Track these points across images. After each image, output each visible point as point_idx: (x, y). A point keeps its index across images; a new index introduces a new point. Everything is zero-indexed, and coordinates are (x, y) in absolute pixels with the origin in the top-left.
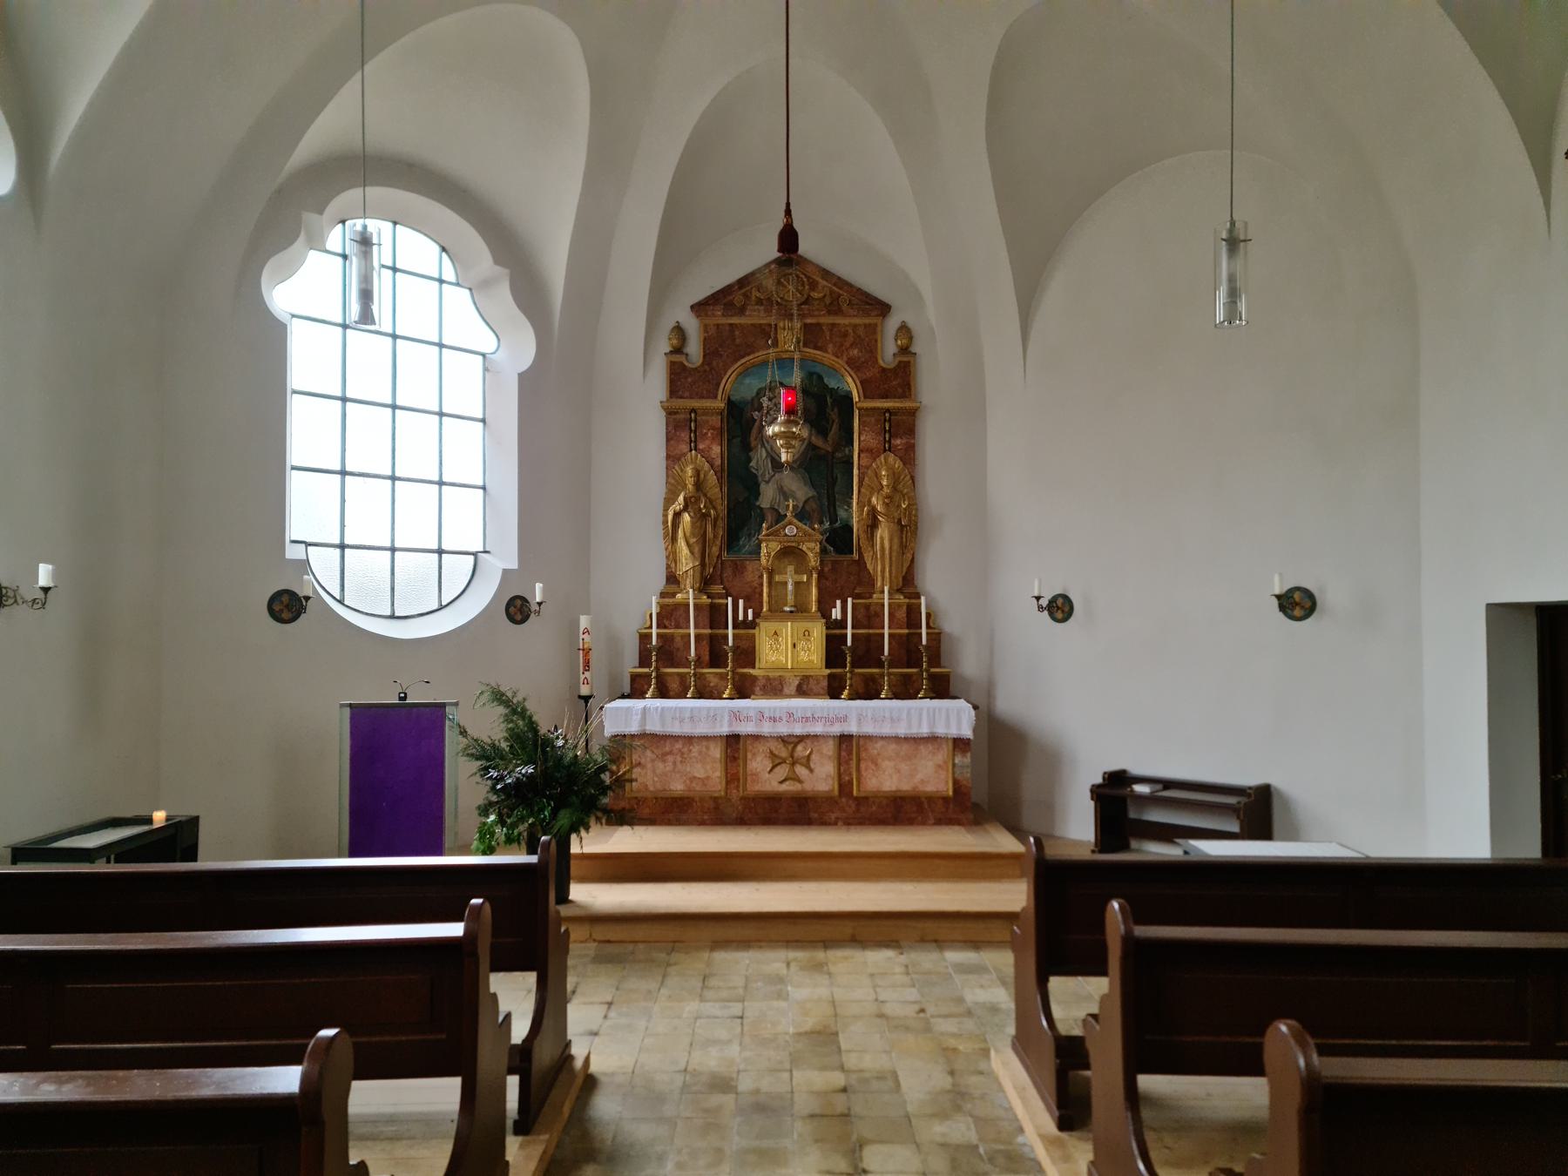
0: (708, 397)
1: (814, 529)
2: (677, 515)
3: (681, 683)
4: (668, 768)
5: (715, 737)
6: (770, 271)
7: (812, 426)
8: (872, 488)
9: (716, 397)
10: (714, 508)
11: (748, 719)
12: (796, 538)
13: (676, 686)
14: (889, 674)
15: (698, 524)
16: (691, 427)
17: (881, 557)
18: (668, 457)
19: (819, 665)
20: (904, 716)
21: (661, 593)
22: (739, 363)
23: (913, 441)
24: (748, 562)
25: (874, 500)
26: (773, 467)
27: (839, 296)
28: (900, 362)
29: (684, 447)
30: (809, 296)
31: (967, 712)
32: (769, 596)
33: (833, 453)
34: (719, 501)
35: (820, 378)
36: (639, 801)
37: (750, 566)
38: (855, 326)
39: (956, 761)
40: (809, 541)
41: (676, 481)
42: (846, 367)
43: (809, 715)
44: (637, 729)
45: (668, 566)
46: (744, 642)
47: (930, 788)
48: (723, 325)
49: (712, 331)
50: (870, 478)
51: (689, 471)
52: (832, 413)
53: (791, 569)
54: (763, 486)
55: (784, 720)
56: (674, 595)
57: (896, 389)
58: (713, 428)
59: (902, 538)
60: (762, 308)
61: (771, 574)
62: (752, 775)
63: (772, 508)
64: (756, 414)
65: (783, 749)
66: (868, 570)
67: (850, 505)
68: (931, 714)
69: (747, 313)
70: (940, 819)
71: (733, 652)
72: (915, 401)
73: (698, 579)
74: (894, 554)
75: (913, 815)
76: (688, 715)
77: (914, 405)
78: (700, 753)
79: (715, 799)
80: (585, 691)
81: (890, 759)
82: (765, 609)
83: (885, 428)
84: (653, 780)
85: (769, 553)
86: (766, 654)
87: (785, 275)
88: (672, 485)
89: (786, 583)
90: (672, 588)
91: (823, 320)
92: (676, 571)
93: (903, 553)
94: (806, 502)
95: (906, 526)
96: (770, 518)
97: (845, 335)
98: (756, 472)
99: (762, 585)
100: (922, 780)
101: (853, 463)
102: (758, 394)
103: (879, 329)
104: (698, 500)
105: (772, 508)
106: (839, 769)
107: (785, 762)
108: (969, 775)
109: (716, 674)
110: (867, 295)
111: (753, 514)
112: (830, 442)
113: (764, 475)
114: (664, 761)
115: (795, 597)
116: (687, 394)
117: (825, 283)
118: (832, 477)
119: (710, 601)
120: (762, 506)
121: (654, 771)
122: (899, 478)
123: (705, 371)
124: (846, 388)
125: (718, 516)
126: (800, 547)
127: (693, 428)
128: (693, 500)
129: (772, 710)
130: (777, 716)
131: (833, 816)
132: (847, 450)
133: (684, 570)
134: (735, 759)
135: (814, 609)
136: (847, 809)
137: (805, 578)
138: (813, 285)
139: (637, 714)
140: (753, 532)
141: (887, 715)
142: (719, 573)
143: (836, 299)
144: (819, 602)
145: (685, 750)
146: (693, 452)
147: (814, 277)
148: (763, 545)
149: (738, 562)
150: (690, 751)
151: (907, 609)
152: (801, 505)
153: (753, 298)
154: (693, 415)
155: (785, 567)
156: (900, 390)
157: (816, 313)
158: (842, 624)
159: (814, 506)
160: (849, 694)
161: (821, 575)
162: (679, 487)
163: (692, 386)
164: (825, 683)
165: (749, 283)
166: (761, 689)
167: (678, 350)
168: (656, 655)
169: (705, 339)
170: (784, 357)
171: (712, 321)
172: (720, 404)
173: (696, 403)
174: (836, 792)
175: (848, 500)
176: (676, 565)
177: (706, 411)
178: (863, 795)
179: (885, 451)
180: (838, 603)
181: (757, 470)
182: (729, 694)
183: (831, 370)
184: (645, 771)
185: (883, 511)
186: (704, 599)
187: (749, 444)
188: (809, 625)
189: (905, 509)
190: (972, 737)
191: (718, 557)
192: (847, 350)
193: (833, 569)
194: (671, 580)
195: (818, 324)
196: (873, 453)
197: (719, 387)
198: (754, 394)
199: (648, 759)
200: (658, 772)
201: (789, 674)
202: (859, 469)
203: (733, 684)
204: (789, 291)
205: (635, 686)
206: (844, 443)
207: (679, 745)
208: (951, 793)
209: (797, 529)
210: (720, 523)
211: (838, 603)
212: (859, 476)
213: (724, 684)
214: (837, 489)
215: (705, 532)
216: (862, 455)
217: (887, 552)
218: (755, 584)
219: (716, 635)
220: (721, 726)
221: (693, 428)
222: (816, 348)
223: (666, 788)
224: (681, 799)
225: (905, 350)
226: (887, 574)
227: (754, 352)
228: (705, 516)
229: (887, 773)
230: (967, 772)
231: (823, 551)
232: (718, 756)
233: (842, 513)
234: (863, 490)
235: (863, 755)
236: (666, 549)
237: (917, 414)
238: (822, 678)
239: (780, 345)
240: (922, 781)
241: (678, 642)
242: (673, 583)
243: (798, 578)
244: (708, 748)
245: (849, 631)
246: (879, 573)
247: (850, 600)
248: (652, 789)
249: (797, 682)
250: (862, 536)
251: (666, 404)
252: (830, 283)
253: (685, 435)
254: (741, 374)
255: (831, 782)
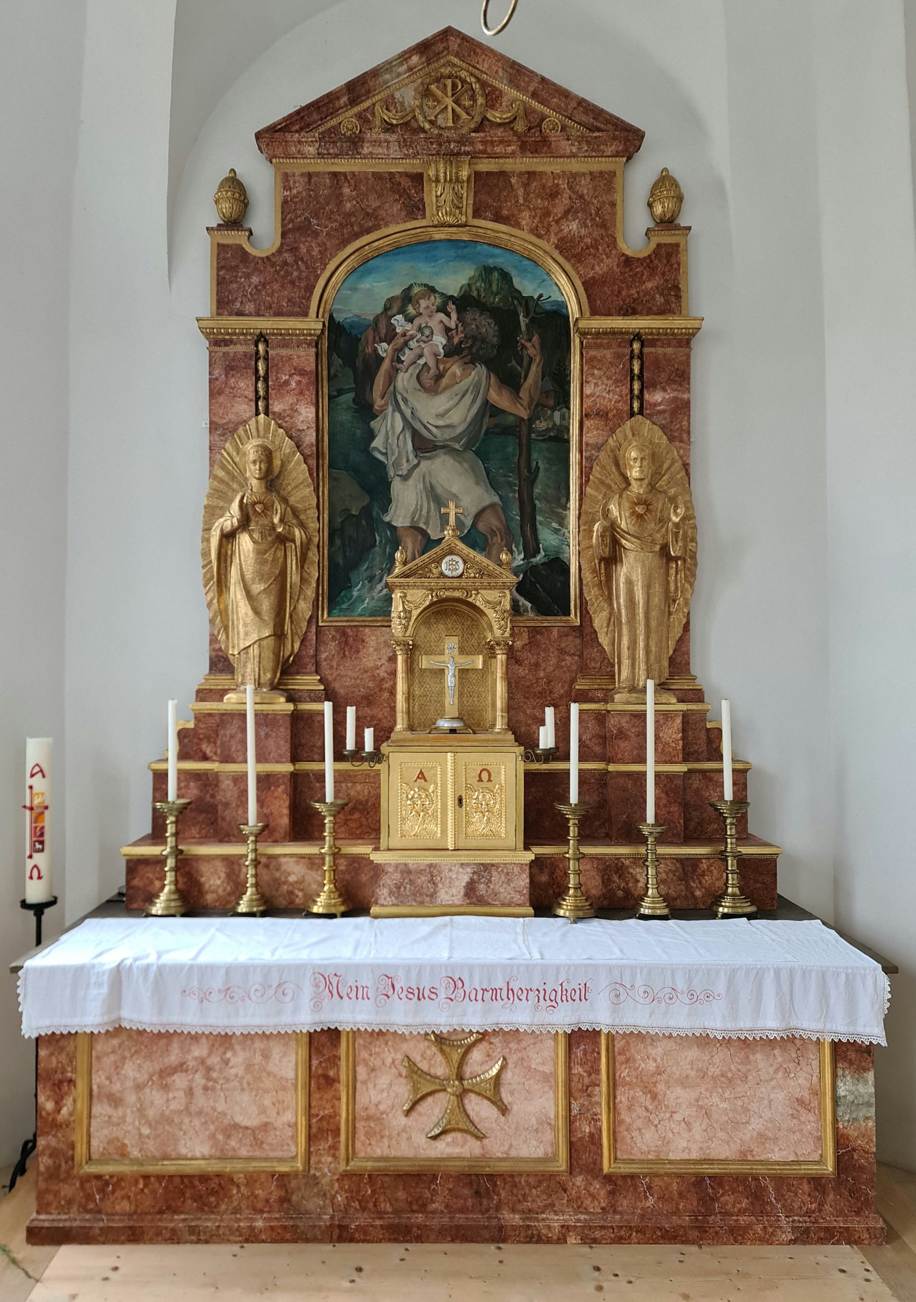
0: (290, 314)
1: (500, 563)
2: (228, 537)
3: (228, 876)
4: (174, 1106)
5: (281, 1036)
6: (410, 69)
7: (489, 369)
8: (609, 487)
9: (305, 314)
10: (302, 525)
11: (358, 992)
12: (463, 582)
13: (219, 882)
14: (658, 859)
15: (269, 556)
16: (257, 370)
17: (629, 621)
18: (214, 427)
19: (511, 842)
20: (721, 987)
21: (199, 691)
22: (350, 249)
23: (685, 396)
24: (367, 630)
25: (614, 509)
26: (416, 448)
27: (543, 118)
28: (659, 246)
29: (244, 409)
30: (485, 119)
31: (870, 981)
32: (409, 697)
33: (531, 420)
34: (313, 513)
35: (506, 277)
36: (107, 1183)
37: (372, 639)
38: (574, 176)
39: (841, 1092)
40: (490, 587)
41: (228, 472)
42: (556, 254)
43: (500, 983)
44: (98, 1020)
45: (213, 640)
46: (359, 787)
47: (778, 1154)
48: (318, 174)
49: (299, 187)
50: (603, 467)
51: (251, 449)
52: (528, 345)
53: (451, 643)
54: (397, 486)
55: (442, 994)
56: (221, 694)
57: (653, 298)
58: (301, 372)
59: (668, 582)
60: (394, 137)
61: (412, 651)
62: (368, 1118)
63: (415, 528)
64: (383, 349)
65: (439, 1058)
66: (600, 645)
67: (562, 521)
68: (786, 988)
69: (366, 151)
70: (807, 1231)
71: (334, 816)
72: (688, 317)
73: (268, 664)
74: (654, 614)
75: (743, 1220)
76: (217, 983)
77: (690, 324)
78: (249, 1067)
79: (282, 1179)
80: (35, 892)
81: (684, 1082)
82: (399, 727)
83: (632, 370)
84: (140, 1135)
85: (408, 613)
86: (403, 819)
87: (438, 80)
88: (221, 481)
89: (442, 671)
90: (222, 681)
91: (509, 165)
92: (227, 647)
93: (670, 613)
94: (478, 516)
95: (676, 559)
96: (410, 547)
97: (554, 194)
98: (381, 458)
99: (394, 673)
100: (761, 1135)
101: (568, 441)
102: (386, 309)
103: (618, 180)
104: (268, 508)
105: (415, 528)
106: (569, 1109)
107: (445, 1090)
108: (871, 1124)
109: (302, 857)
110: (597, 113)
111: (377, 538)
112: (525, 402)
113: (397, 465)
114: (166, 1088)
115: (461, 695)
116: (250, 307)
117: (514, 93)
118: (529, 467)
119: (291, 707)
120: (394, 524)
121: (141, 1112)
122: (661, 466)
123: (285, 263)
124: (556, 297)
125: (310, 540)
126: (470, 600)
127: (261, 372)
128: (258, 508)
129: (414, 974)
130: (426, 984)
131: (555, 1221)
132: (557, 415)
133: (242, 647)
134: (330, 1082)
135: (500, 725)
136: (588, 1202)
137: (479, 661)
138: (493, 98)
139: (99, 985)
140: (378, 572)
141: (681, 985)
142: (312, 652)
143: (536, 123)
144: (511, 707)
145: (214, 1060)
146: (262, 416)
147: (496, 83)
148: (397, 595)
149: (349, 630)
150: (227, 1062)
151: (683, 722)
152: (468, 522)
153: (378, 123)
154: (261, 347)
155: (440, 640)
156: (659, 299)
157: (498, 149)
158: (560, 753)
159: (495, 523)
160: (577, 908)
161: (513, 656)
162: (235, 486)
163: (259, 291)
164: (523, 881)
165: (368, 93)
166: (391, 893)
167: (234, 223)
168: (176, 822)
169: (285, 202)
170: (437, 237)
171: (299, 167)
172: (313, 324)
173: (266, 324)
174: (562, 1165)
175: (560, 511)
176: (227, 637)
177: (287, 339)
178: (625, 1169)
179: (632, 414)
180: (549, 712)
181: (385, 454)
182: (328, 905)
183: (526, 262)
184: (120, 1111)
185: (632, 529)
186: (282, 705)
187: (371, 406)
188: (489, 759)
189: (677, 525)
190: (884, 1043)
191: (310, 621)
192: (557, 222)
193: (532, 644)
194: (220, 666)
195: (502, 174)
196: (607, 419)
197: (312, 293)
198: (379, 310)
199: (129, 1084)
200: (151, 1113)
201: (450, 860)
202: (581, 451)
203: (335, 882)
204: (446, 107)
205: (136, 882)
206: (551, 402)
207: (199, 1051)
208: (830, 1167)
209: (465, 562)
210: (313, 555)
211: (549, 712)
212: (581, 463)
213: (315, 876)
214: (537, 491)
215: (283, 574)
216: (587, 423)
217: (641, 611)
218: (382, 673)
219: (306, 774)
220: (296, 1010)
221: (261, 372)
222: (498, 218)
223: (169, 1150)
224: (204, 1178)
225: (668, 223)
226: (641, 654)
227: (377, 227)
228: (283, 540)
229: (677, 1117)
230: (867, 1118)
231: (516, 608)
232: (291, 1075)
233: (547, 537)
234: (589, 490)
235: (624, 1073)
236: (209, 605)
237: (693, 343)
238: (516, 870)
239: (428, 214)
240: (762, 1138)
241: (227, 788)
242: (221, 671)
243: (466, 661)
244: (266, 1056)
245: (574, 766)
246: (625, 652)
247: (574, 708)
248: (135, 1153)
249: (465, 879)
250: (588, 576)
251: (204, 324)
252: (524, 90)
253: (245, 385)
254: (353, 271)
255: (548, 1136)
